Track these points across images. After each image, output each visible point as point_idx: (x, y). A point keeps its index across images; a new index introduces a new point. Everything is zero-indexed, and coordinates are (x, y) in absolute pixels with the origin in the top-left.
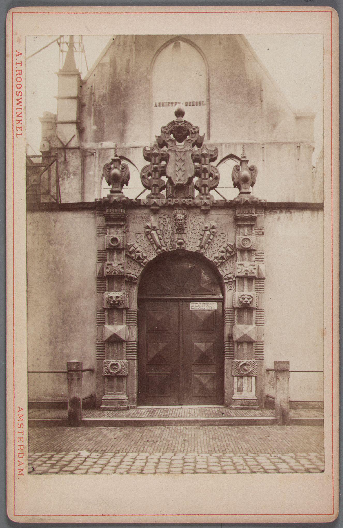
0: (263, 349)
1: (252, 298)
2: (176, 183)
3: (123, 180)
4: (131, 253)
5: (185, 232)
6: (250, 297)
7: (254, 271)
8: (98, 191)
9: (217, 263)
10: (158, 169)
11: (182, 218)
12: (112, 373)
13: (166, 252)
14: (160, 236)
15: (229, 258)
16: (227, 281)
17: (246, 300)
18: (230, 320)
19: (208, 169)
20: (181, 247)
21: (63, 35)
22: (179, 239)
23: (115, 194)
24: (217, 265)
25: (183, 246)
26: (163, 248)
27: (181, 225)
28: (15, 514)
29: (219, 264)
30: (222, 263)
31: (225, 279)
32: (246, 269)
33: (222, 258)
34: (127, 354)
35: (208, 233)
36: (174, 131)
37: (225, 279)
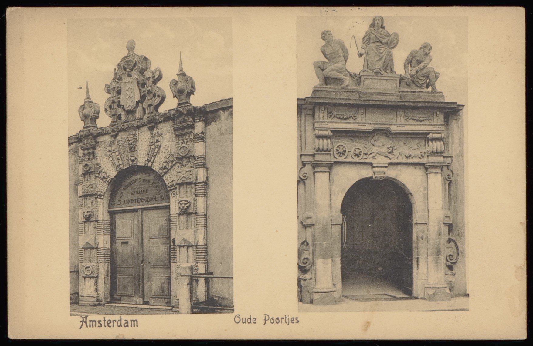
0: (93, 327)
1: (188, 202)
2: (127, 109)
3: (91, 117)
4: (99, 174)
5: (136, 150)
6: (186, 202)
7: (191, 177)
8: (437, 94)
9: (161, 173)
10: (115, 101)
11: (131, 139)
12: (86, 274)
13: (124, 169)
14: (118, 157)
15: (172, 167)
16: (170, 189)
17: (183, 205)
18: (104, 259)
19: (151, 91)
20: (133, 163)
21: (464, 104)
22: (131, 157)
23: (355, 102)
24: (162, 175)
25: (135, 162)
26: (121, 166)
27: (132, 144)
28: (316, 174)
29: (163, 174)
30: (166, 173)
31: (168, 187)
32: (183, 176)
33: (165, 168)
34: (98, 259)
35: (153, 147)
36: (126, 65)
37: (168, 187)
